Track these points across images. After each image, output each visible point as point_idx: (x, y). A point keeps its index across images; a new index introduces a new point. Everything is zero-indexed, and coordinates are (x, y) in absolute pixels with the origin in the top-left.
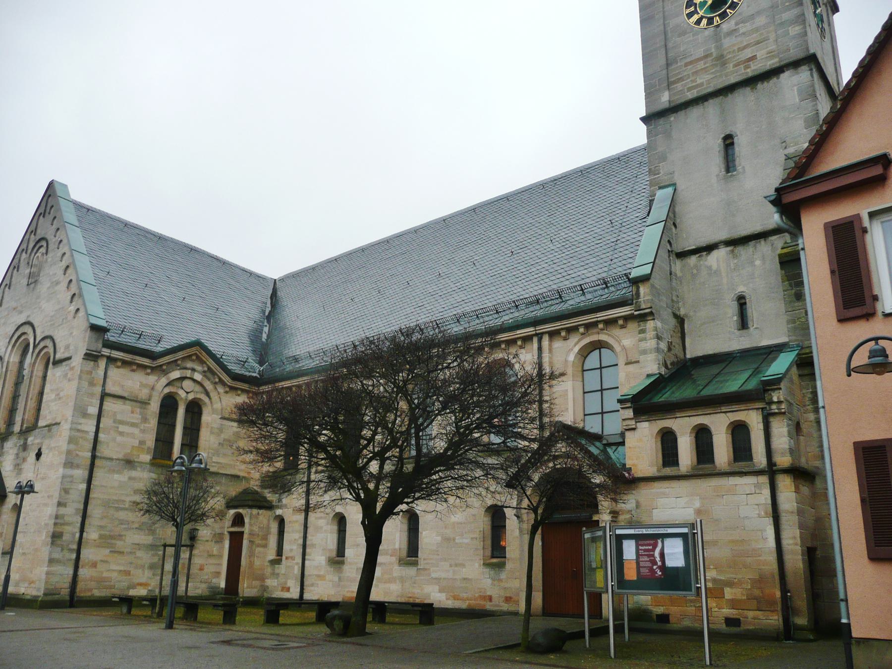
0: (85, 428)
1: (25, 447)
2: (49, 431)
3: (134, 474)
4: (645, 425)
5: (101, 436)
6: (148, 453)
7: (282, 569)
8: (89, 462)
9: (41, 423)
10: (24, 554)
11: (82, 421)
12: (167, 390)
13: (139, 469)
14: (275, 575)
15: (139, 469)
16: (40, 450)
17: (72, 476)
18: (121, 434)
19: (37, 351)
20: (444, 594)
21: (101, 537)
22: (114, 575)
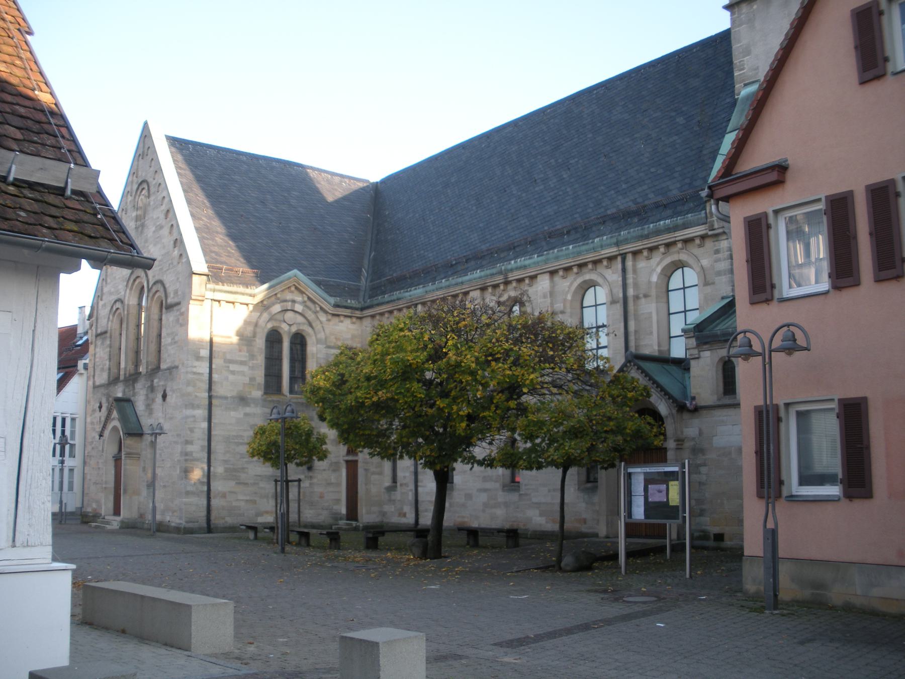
0: (200, 370)
1: (152, 389)
2: (170, 373)
3: (248, 410)
4: (707, 354)
5: (215, 376)
6: (258, 389)
7: (397, 495)
8: (206, 402)
9: (163, 366)
10: (165, 486)
11: (197, 363)
12: (270, 326)
13: (252, 405)
14: (391, 501)
15: (252, 405)
16: (165, 391)
17: (194, 416)
18: (233, 373)
19: (151, 295)
20: (544, 518)
21: (226, 470)
22: (242, 504)
